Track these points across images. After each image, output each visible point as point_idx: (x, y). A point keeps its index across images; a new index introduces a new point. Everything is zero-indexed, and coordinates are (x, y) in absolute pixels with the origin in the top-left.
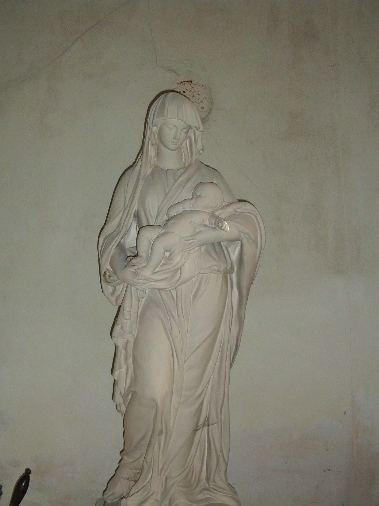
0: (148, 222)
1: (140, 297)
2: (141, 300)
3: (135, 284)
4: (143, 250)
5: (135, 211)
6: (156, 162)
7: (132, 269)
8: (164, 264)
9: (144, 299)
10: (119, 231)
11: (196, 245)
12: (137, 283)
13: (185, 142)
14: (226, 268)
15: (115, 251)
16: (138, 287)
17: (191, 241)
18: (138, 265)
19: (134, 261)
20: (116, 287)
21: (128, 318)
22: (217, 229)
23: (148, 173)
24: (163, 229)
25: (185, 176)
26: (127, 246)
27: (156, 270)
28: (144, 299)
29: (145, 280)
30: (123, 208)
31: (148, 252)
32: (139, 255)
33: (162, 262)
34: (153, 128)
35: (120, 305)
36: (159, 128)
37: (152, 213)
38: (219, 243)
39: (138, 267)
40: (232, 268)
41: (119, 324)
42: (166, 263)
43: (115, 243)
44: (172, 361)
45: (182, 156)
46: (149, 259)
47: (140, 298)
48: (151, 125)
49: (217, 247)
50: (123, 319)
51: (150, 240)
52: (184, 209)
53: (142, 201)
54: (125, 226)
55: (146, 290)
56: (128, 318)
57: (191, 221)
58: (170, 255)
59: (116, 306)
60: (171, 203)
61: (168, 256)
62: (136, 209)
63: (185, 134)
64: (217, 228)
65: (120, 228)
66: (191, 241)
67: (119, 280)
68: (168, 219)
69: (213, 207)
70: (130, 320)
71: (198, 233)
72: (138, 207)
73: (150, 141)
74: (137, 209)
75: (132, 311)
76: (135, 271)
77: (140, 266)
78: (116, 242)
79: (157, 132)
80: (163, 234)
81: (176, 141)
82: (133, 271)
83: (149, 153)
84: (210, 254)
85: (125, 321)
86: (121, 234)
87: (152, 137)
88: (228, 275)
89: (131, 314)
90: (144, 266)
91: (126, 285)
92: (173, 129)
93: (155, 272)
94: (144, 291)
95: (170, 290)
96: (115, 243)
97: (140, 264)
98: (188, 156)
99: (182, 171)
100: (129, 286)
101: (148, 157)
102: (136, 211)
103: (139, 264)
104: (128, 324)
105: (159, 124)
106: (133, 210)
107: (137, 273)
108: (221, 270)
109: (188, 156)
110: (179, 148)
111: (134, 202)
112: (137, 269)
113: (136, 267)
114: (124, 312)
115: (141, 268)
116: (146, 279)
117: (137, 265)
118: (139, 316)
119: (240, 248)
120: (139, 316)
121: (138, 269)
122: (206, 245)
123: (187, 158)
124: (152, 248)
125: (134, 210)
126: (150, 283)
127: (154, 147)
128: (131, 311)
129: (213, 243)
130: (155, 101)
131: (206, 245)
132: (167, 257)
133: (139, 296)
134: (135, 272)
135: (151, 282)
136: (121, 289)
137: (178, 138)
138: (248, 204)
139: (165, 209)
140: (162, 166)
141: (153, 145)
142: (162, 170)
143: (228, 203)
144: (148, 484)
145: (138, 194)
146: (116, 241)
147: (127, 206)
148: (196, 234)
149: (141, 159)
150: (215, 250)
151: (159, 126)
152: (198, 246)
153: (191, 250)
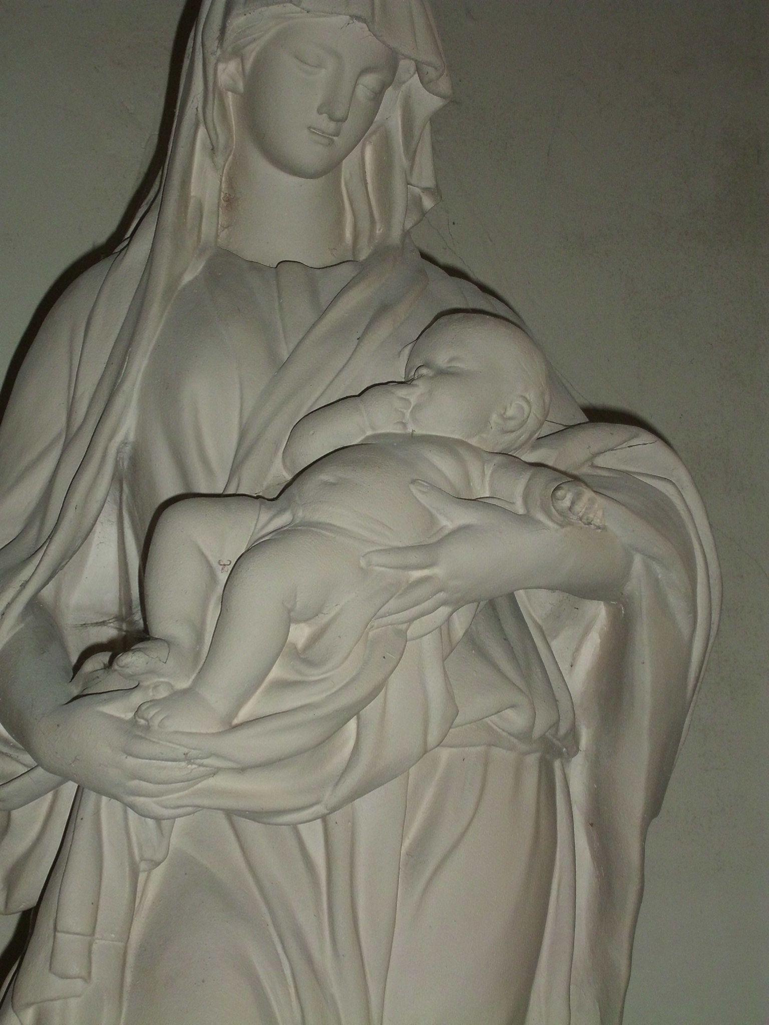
0: (183, 470)
1: (142, 859)
2: (142, 877)
3: (135, 783)
5: (124, 443)
6: (223, 234)
7: (120, 709)
8: (283, 685)
9: (158, 874)
10: (37, 540)
11: (442, 595)
12: (140, 779)
13: (358, 148)
14: (556, 725)
15: (17, 629)
16: (142, 799)
17: (417, 574)
19: (132, 661)
20: (9, 815)
21: (75, 969)
22: (539, 522)
23: (187, 278)
24: (282, 511)
25: (356, 297)
26: (69, 619)
27: (243, 714)
28: (158, 874)
29: (183, 764)
30: (60, 434)
31: (203, 622)
33: (276, 673)
34: (221, 66)
35: (33, 902)
36: (248, 65)
37: (212, 453)
40: (574, 733)
41: (28, 1005)
42: (298, 678)
43: (19, 593)
45: (341, 211)
47: (143, 866)
48: (212, 44)
50: (52, 977)
51: (215, 564)
52: (373, 428)
54: (71, 514)
55: (174, 818)
56: (75, 969)
57: (415, 477)
58: (315, 639)
59: (7, 912)
60: (310, 403)
61: (301, 643)
62: (126, 437)
64: (541, 517)
65: (42, 523)
66: (417, 574)
67: (40, 770)
68: (289, 477)
69: (512, 424)
70: (87, 978)
71: (449, 534)
72: (142, 427)
73: (202, 132)
74: (132, 437)
75: (97, 935)
76: (130, 715)
78: (24, 586)
79: (241, 86)
80: (282, 533)
81: (332, 125)
82: (123, 716)
83: (194, 190)
84: (481, 653)
85: (57, 985)
86: (55, 549)
87: (214, 113)
88: (557, 764)
89: (94, 946)
90: (185, 692)
91: (70, 788)
92: (319, 66)
93: (236, 721)
94: (165, 823)
95: (294, 827)
96: (19, 593)
97: (162, 680)
98: (373, 222)
99: (347, 272)
100: (90, 798)
101: (186, 207)
102: (128, 449)
103: (156, 680)
104: (73, 1002)
105: (250, 43)
106: (111, 438)
107: (148, 728)
108: (537, 733)
109: (373, 222)
110: (332, 168)
111: (120, 401)
112: (143, 708)
113: (137, 698)
114: (59, 935)
115: (164, 698)
116: (193, 753)
117: (146, 684)
118: (131, 959)
119: (599, 641)
120: (131, 959)
121: (154, 702)
122: (473, 602)
123: (365, 225)
124: (224, 600)
125: (119, 438)
126: (211, 782)
127: (220, 160)
128: (93, 934)
129: (492, 604)
131: (475, 604)
132: (296, 648)
133: (137, 858)
134: (134, 723)
135: (216, 771)
136: (37, 827)
137: (339, 114)
138: (646, 437)
139: (281, 426)
140: (251, 254)
141: (213, 150)
142: (255, 266)
143: (562, 428)
146: (27, 582)
147: (80, 428)
148: (440, 542)
151: (254, 54)
152: (444, 603)
153: (411, 621)
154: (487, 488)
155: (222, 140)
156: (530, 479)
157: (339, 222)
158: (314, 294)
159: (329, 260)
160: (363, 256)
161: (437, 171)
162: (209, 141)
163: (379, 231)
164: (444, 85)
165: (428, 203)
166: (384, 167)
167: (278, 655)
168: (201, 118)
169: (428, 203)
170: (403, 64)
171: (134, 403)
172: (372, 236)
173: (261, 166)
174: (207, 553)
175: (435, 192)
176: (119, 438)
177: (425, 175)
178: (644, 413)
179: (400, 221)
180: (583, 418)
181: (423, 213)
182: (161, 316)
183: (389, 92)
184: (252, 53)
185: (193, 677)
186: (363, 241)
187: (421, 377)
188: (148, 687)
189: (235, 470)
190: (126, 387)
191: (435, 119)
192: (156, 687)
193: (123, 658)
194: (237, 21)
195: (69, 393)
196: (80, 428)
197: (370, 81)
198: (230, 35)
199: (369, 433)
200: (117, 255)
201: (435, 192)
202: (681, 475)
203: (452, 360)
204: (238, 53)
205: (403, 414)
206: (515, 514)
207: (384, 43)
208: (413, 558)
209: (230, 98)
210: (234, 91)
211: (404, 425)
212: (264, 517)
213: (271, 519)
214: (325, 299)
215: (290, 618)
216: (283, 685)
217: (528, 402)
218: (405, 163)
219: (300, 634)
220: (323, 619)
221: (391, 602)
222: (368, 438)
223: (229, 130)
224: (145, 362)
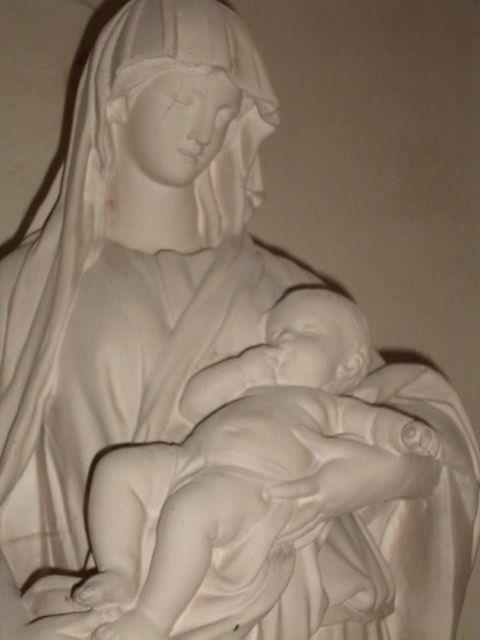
4: (113, 552)
5: (49, 396)
8: (211, 600)
11: (321, 515)
18: (101, 612)
21: (175, 165)
23: (88, 264)
24: (194, 457)
32: (103, 569)
33: (203, 590)
36: (132, 103)
37: (122, 405)
38: (351, 516)
39: (104, 617)
42: (219, 593)
44: (219, 413)
46: (142, 586)
49: (348, 525)
53: (82, 356)
58: (229, 561)
62: (50, 391)
63: (244, 369)
72: (63, 383)
74: (54, 392)
77: (113, 613)
79: (124, 118)
83: (87, 196)
87: (103, 140)
90: (132, 613)
106: (39, 394)
113: (92, 622)
121: (108, 625)
123: (214, 220)
125: (45, 394)
130: (466, 411)
141: (102, 166)
142: (139, 254)
144: (202, 366)
145: (58, 337)
147: (13, 381)
149: (57, 221)
150: (343, 528)
154: (341, 425)
155: (109, 158)
156: (376, 420)
157: (194, 220)
158: (188, 277)
159: (190, 247)
160: (216, 243)
161: (264, 180)
162: (98, 159)
163: (225, 223)
164: (276, 118)
165: (257, 202)
166: (227, 177)
167: (205, 573)
168: (93, 143)
169: (257, 202)
170: (246, 101)
171: (56, 361)
172: (220, 227)
173: (139, 178)
174: (138, 493)
175: (263, 195)
176: (45, 394)
177: (257, 184)
178: (434, 357)
179: (240, 216)
180: (380, 361)
181: (254, 210)
182: (72, 297)
183: (234, 124)
184: (135, 94)
185: (136, 600)
186: (214, 233)
187: (284, 341)
188: (101, 612)
189: (142, 419)
190: (49, 354)
191: (266, 145)
192: (108, 612)
193: (84, 593)
194: (125, 71)
195: (347, 561)
196: (13, 381)
197: (224, 114)
198: (118, 82)
199: (249, 386)
200: (28, 248)
201: (263, 195)
202: (454, 399)
203: (307, 326)
204: (124, 94)
205: (274, 371)
206: (366, 446)
207: (234, 83)
208: (302, 488)
209: (115, 127)
210: (118, 122)
211: (274, 377)
212: (182, 462)
213: (186, 465)
214: (196, 278)
215: (211, 542)
216: (211, 600)
217: (362, 355)
218: (244, 173)
219: (219, 555)
220: (236, 544)
221: (288, 525)
222: (249, 390)
223: (114, 153)
224: (63, 334)
